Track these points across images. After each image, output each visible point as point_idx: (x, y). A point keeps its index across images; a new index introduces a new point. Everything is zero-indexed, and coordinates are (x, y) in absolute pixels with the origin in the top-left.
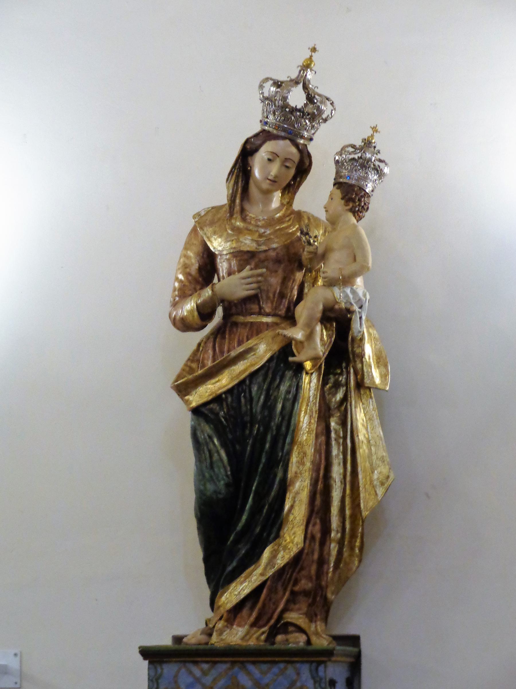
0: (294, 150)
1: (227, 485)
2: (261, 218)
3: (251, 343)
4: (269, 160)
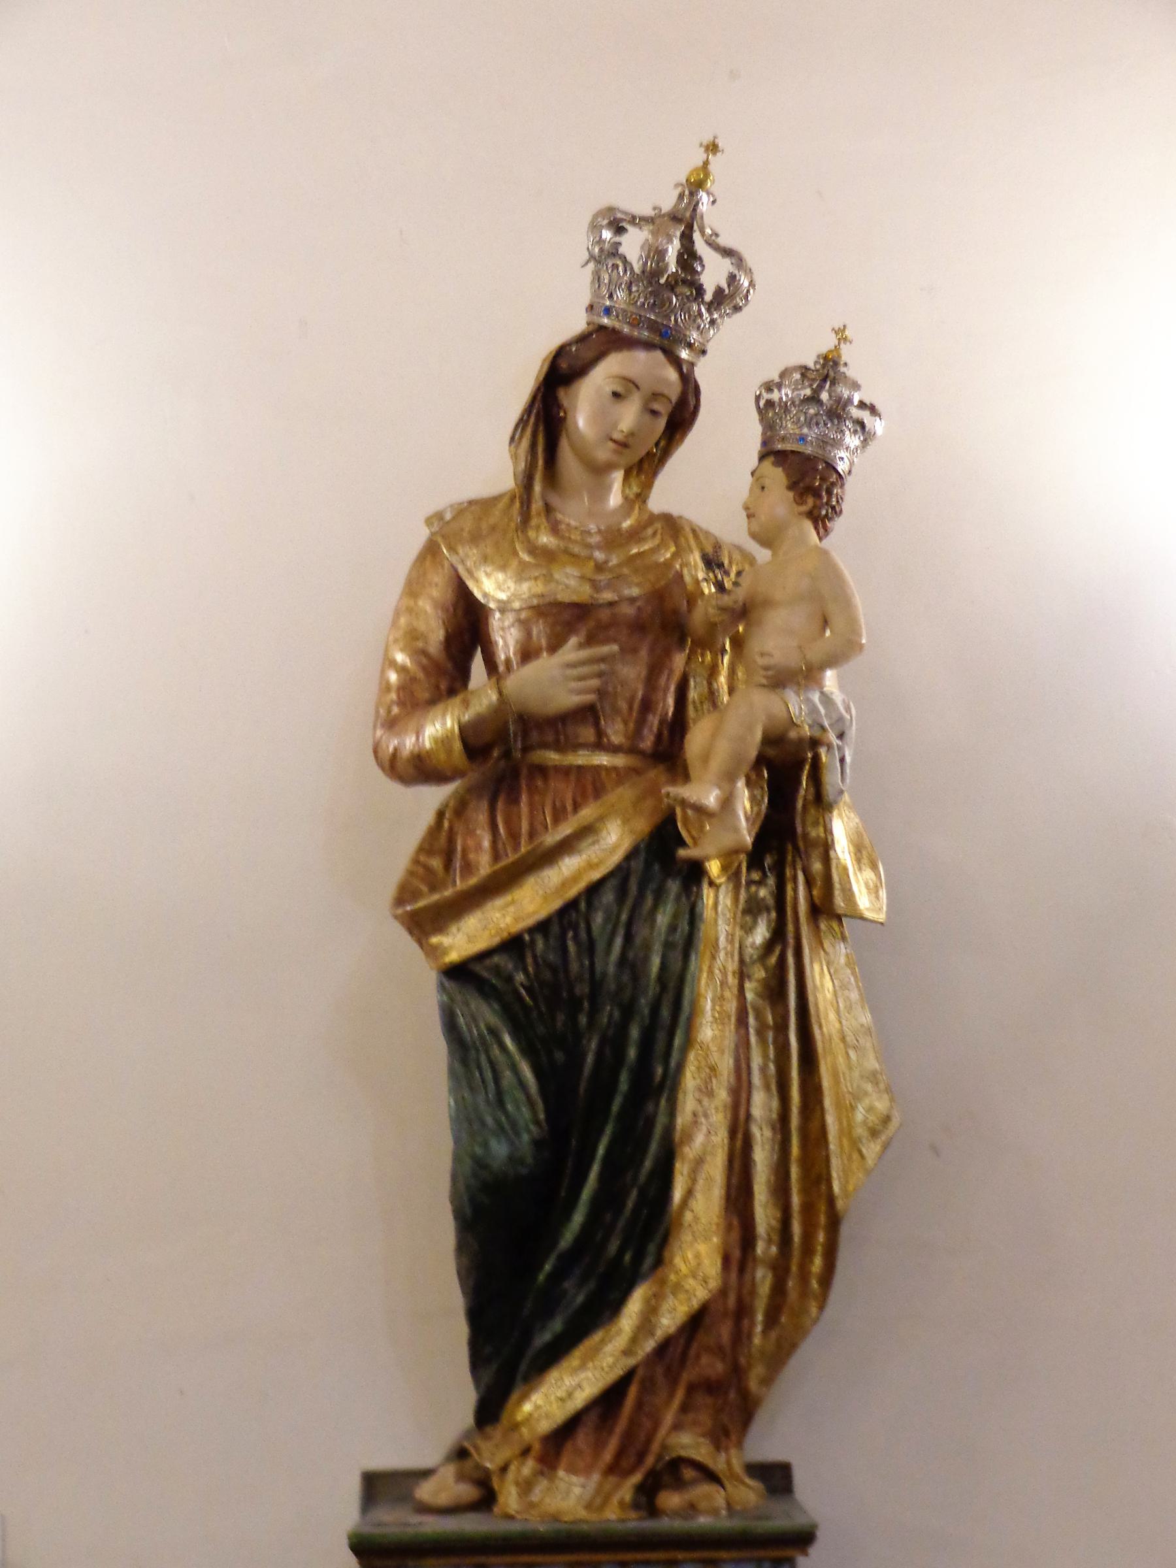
0: (672, 375)
1: (537, 1144)
2: (593, 527)
3: (587, 813)
4: (616, 395)
